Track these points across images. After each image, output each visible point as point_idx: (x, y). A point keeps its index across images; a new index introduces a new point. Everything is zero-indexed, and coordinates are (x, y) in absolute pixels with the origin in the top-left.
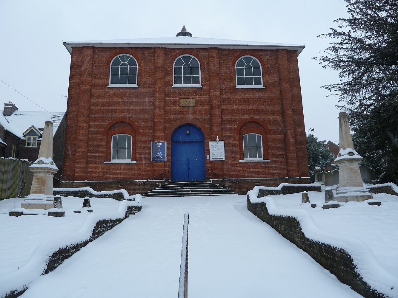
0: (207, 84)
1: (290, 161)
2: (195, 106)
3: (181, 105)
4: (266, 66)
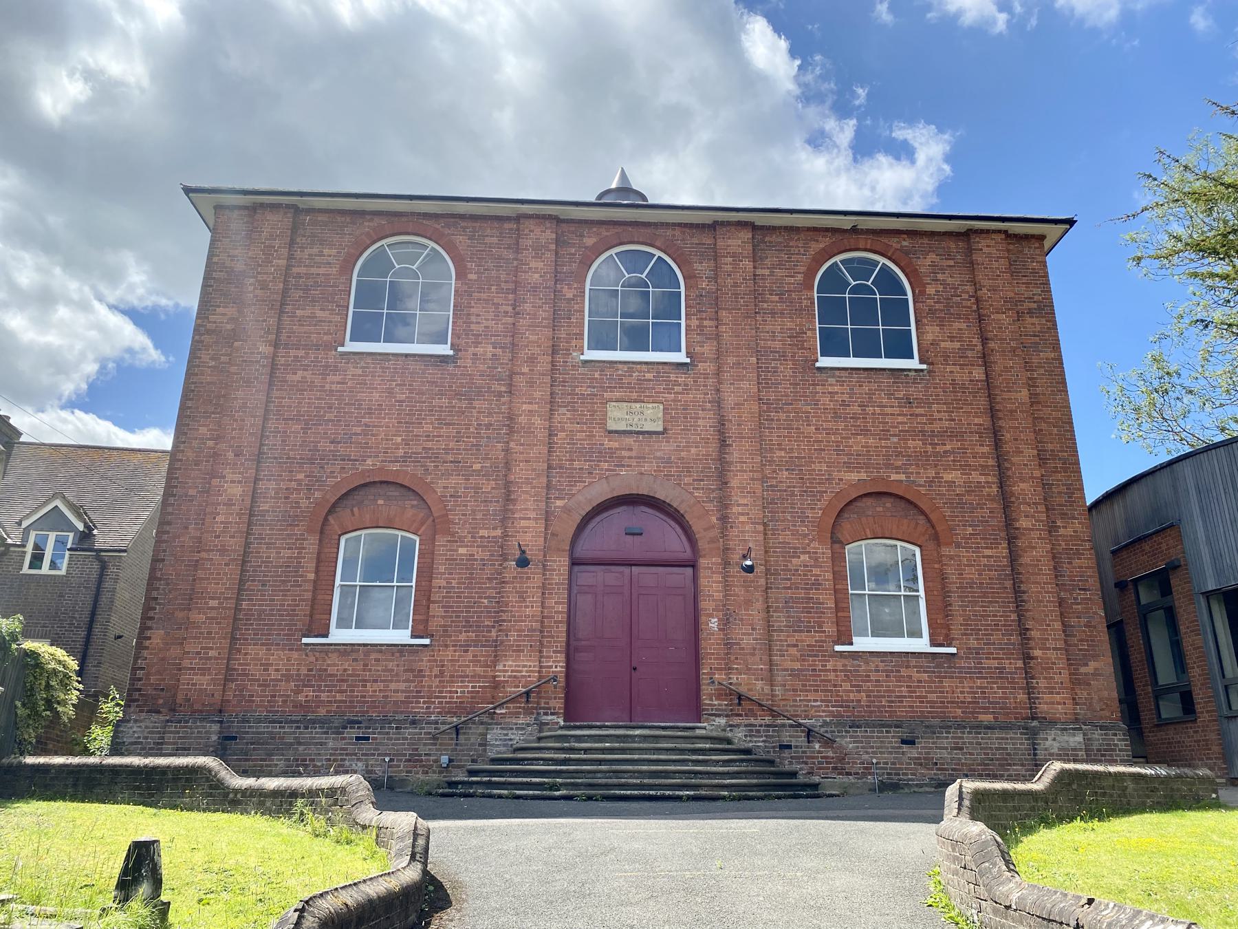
0: (708, 349)
1: (1037, 653)
2: (665, 430)
3: (612, 426)
4: (930, 290)
